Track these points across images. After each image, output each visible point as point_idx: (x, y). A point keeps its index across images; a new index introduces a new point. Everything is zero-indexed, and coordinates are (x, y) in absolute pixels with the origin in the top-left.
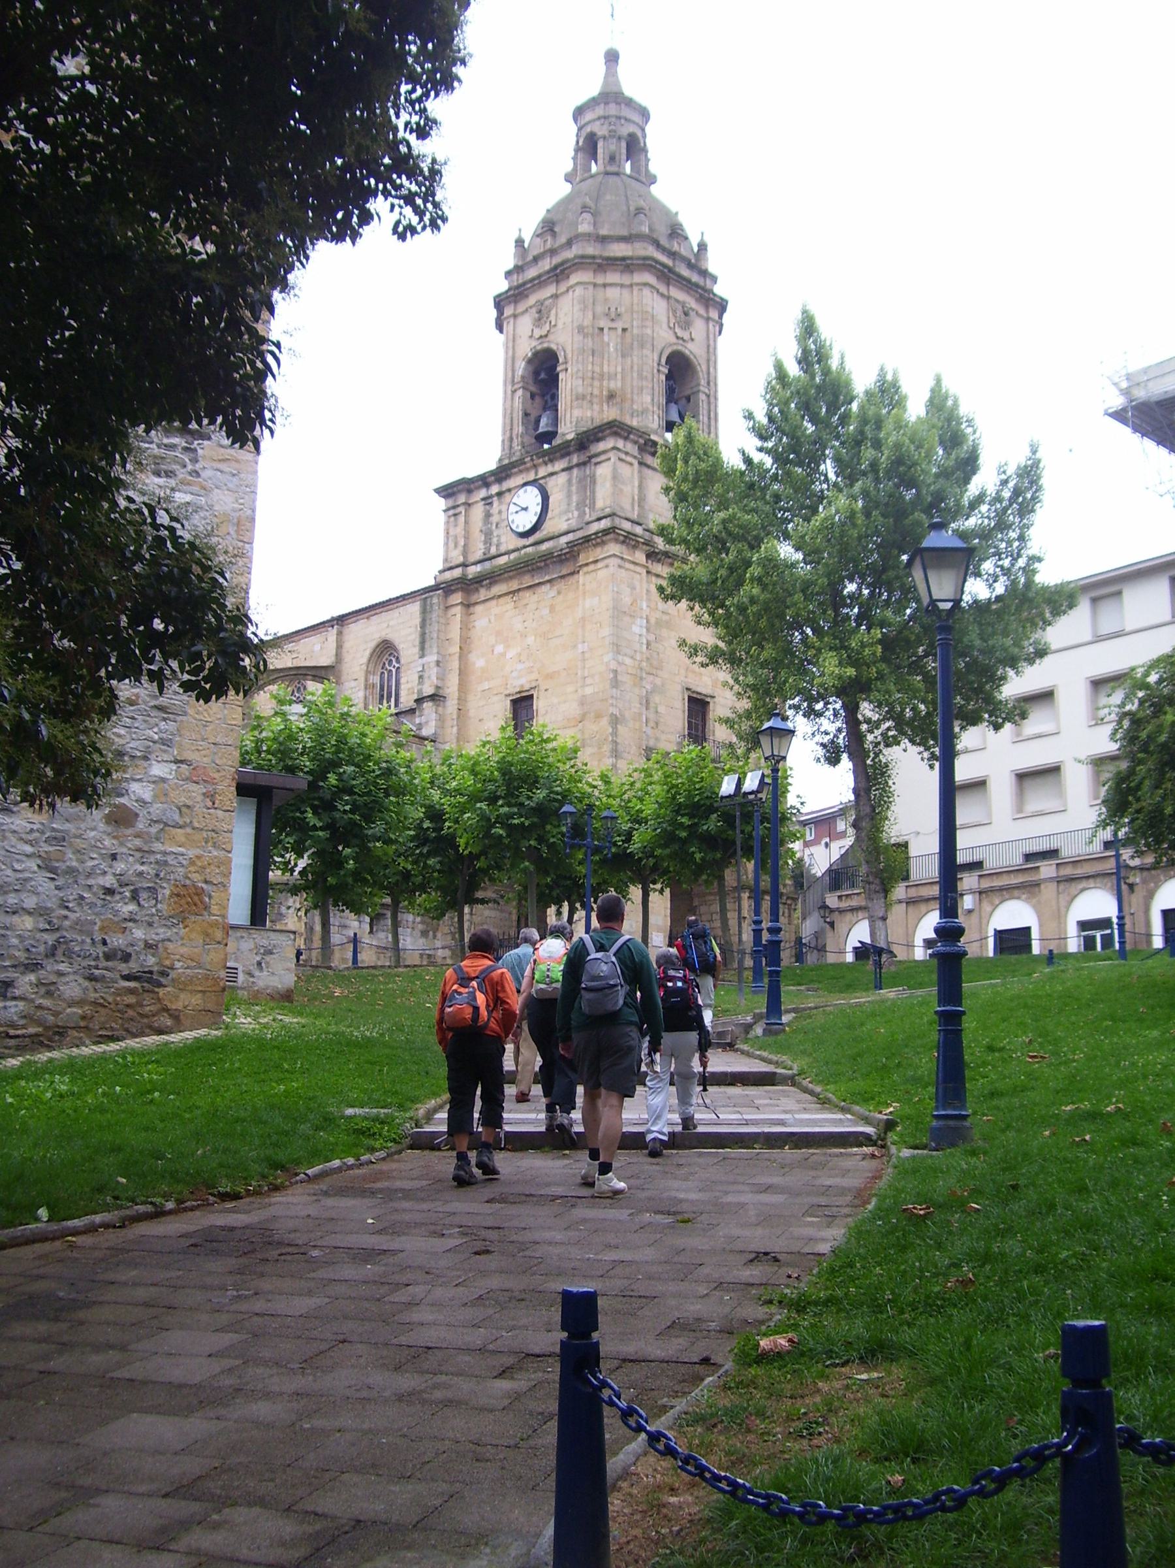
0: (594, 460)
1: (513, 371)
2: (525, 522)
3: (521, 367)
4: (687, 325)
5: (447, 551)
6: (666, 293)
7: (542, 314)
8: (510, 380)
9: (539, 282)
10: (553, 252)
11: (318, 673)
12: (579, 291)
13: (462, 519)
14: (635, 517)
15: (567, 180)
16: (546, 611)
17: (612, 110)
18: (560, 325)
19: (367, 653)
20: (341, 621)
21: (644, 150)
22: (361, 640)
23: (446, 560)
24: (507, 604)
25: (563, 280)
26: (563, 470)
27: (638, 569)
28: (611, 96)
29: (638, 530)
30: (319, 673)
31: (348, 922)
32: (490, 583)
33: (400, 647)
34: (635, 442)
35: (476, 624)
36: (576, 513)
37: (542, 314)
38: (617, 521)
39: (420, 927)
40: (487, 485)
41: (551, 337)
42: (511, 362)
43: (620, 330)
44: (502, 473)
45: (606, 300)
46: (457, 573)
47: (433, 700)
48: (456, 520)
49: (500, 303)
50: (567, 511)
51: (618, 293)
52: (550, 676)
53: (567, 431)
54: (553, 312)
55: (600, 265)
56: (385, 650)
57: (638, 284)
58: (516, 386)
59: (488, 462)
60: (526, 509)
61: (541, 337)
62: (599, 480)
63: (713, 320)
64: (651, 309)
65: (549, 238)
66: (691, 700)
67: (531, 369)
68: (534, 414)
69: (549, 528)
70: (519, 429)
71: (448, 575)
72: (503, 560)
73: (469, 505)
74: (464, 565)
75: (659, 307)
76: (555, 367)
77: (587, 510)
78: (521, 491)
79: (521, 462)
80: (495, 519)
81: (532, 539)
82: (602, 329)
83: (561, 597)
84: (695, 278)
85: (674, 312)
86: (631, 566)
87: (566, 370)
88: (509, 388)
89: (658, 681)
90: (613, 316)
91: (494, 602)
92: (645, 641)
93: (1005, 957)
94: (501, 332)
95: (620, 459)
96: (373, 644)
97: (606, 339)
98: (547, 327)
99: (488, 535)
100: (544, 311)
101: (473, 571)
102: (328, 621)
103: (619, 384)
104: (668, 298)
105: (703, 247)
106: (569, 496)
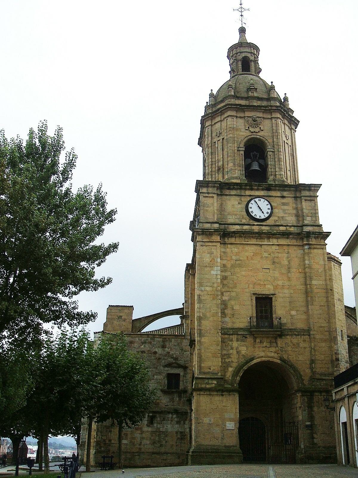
28: (243, 44)
39: (176, 419)
55: (212, 117)
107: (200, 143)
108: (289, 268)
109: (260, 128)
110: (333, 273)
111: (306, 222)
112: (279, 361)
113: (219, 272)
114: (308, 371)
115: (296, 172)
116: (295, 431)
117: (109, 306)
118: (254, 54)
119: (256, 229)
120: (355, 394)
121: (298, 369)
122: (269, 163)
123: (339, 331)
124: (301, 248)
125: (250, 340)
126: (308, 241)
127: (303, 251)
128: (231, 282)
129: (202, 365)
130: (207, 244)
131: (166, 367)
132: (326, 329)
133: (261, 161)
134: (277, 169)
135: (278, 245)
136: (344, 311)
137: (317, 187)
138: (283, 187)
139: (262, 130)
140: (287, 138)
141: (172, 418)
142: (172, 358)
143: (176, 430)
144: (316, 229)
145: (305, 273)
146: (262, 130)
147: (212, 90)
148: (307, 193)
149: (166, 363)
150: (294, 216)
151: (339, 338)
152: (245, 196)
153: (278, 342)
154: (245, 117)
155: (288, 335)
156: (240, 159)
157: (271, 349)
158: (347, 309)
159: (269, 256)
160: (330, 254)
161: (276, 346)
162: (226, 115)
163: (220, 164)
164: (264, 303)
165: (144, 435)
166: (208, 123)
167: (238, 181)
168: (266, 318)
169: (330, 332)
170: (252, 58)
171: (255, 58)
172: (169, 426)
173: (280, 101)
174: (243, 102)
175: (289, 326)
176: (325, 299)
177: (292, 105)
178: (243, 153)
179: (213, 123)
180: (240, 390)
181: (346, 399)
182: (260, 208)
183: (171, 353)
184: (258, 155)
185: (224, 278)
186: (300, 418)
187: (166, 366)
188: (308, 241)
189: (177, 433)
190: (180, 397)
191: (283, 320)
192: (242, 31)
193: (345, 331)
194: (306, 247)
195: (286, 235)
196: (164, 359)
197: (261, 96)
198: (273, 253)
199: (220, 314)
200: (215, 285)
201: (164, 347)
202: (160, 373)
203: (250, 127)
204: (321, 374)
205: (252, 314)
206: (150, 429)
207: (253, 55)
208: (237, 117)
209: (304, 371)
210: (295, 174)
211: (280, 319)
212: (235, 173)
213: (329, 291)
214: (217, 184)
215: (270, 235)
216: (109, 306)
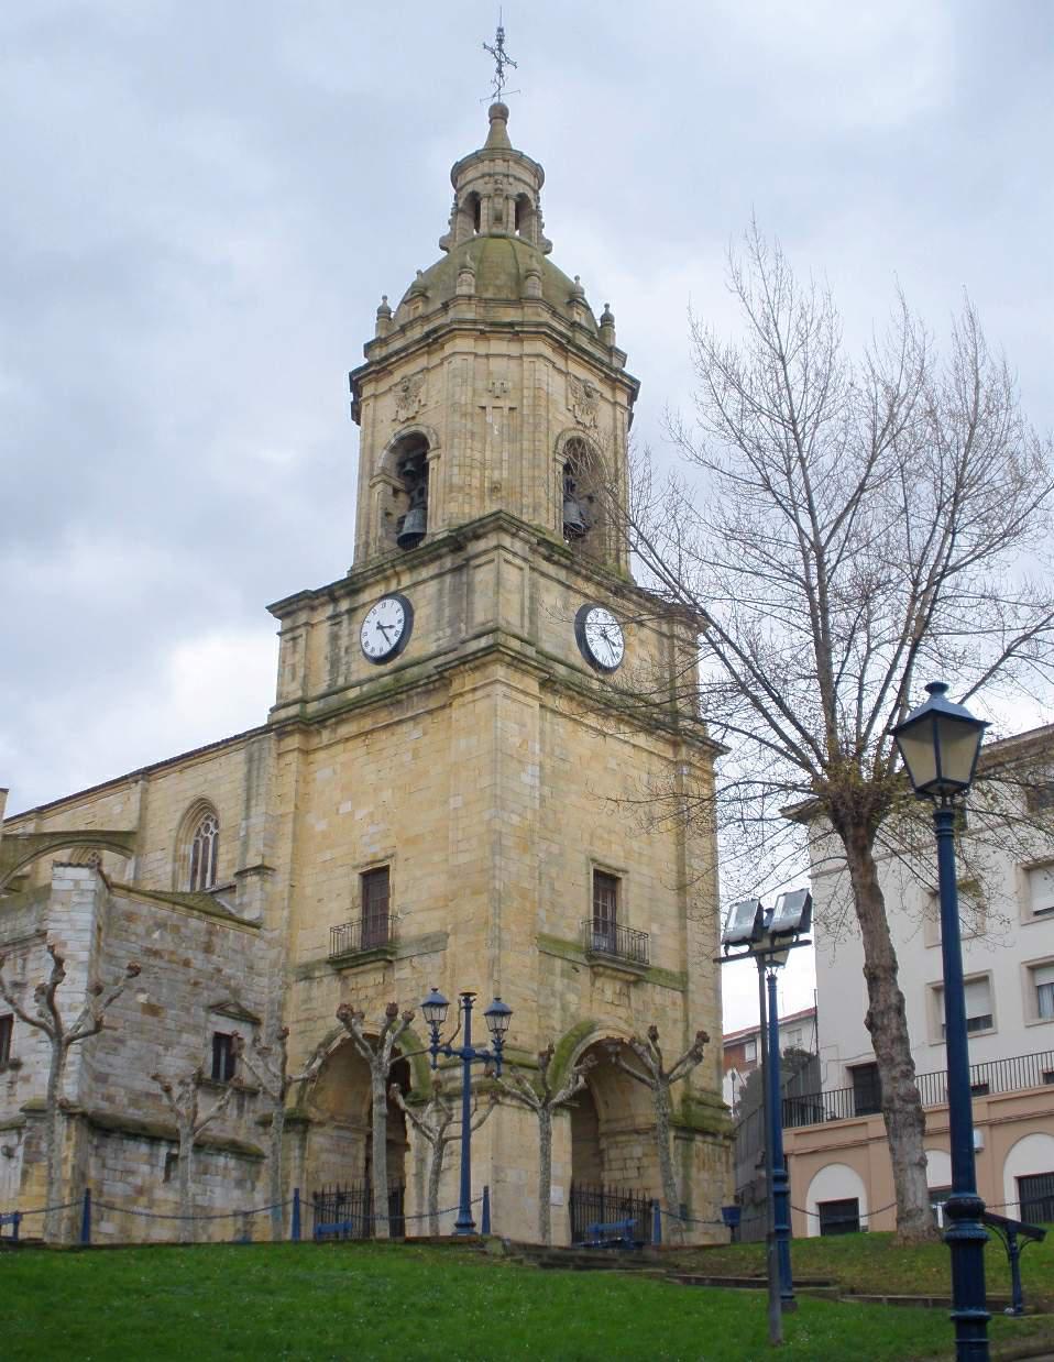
0: (474, 562)
1: (372, 463)
2: (378, 644)
3: (382, 458)
4: (591, 409)
5: (280, 684)
6: (563, 369)
7: (407, 391)
8: (368, 476)
9: (405, 354)
10: (425, 318)
11: (116, 840)
12: (457, 361)
13: (301, 642)
14: (525, 636)
15: (442, 248)
16: (407, 757)
17: (500, 166)
18: (432, 404)
19: (178, 815)
20: (148, 773)
21: (537, 214)
22: (171, 798)
23: (279, 696)
24: (357, 749)
25: (436, 350)
26: (432, 578)
27: (529, 700)
28: (497, 148)
29: (530, 651)
30: (121, 841)
31: (133, 1166)
32: (337, 723)
33: (220, 806)
34: (527, 542)
35: (317, 775)
36: (448, 631)
37: (407, 391)
38: (502, 638)
40: (334, 600)
41: (420, 419)
42: (368, 452)
43: (506, 410)
44: (351, 586)
45: (490, 374)
46: (293, 710)
47: (259, 873)
48: (294, 646)
49: (357, 381)
50: (438, 628)
51: (502, 362)
52: (412, 841)
53: (437, 529)
54: (423, 389)
56: (203, 810)
57: (529, 355)
58: (375, 480)
59: (338, 567)
60: (380, 627)
61: (408, 419)
62: (479, 588)
63: (622, 406)
64: (552, 382)
65: (420, 304)
66: (597, 874)
67: (395, 458)
68: (397, 514)
69: (414, 650)
70: (377, 531)
71: (283, 714)
72: (352, 694)
73: (312, 625)
74: (303, 701)
75: (556, 385)
76: (425, 454)
77: (463, 626)
78: (378, 607)
79: (380, 569)
80: (344, 642)
81: (390, 666)
82: (484, 408)
83: (426, 740)
84: (598, 353)
85: (575, 391)
86: (521, 697)
87: (439, 457)
88: (366, 482)
89: (555, 849)
90: (498, 392)
91: (340, 747)
92: (537, 795)
93: (831, 1239)
94: (358, 423)
95: (507, 561)
96: (187, 804)
97: (489, 419)
98: (416, 406)
99: (334, 663)
100: (412, 389)
101: (312, 708)
102: (132, 775)
103: (505, 474)
104: (567, 374)
105: (607, 319)
106: (440, 610)
125: (584, 976)
141: (226, 1168)
149: (212, 1002)
172: (218, 1191)
183: (227, 971)
196: (207, 988)
201: (208, 949)
202: (197, 1029)
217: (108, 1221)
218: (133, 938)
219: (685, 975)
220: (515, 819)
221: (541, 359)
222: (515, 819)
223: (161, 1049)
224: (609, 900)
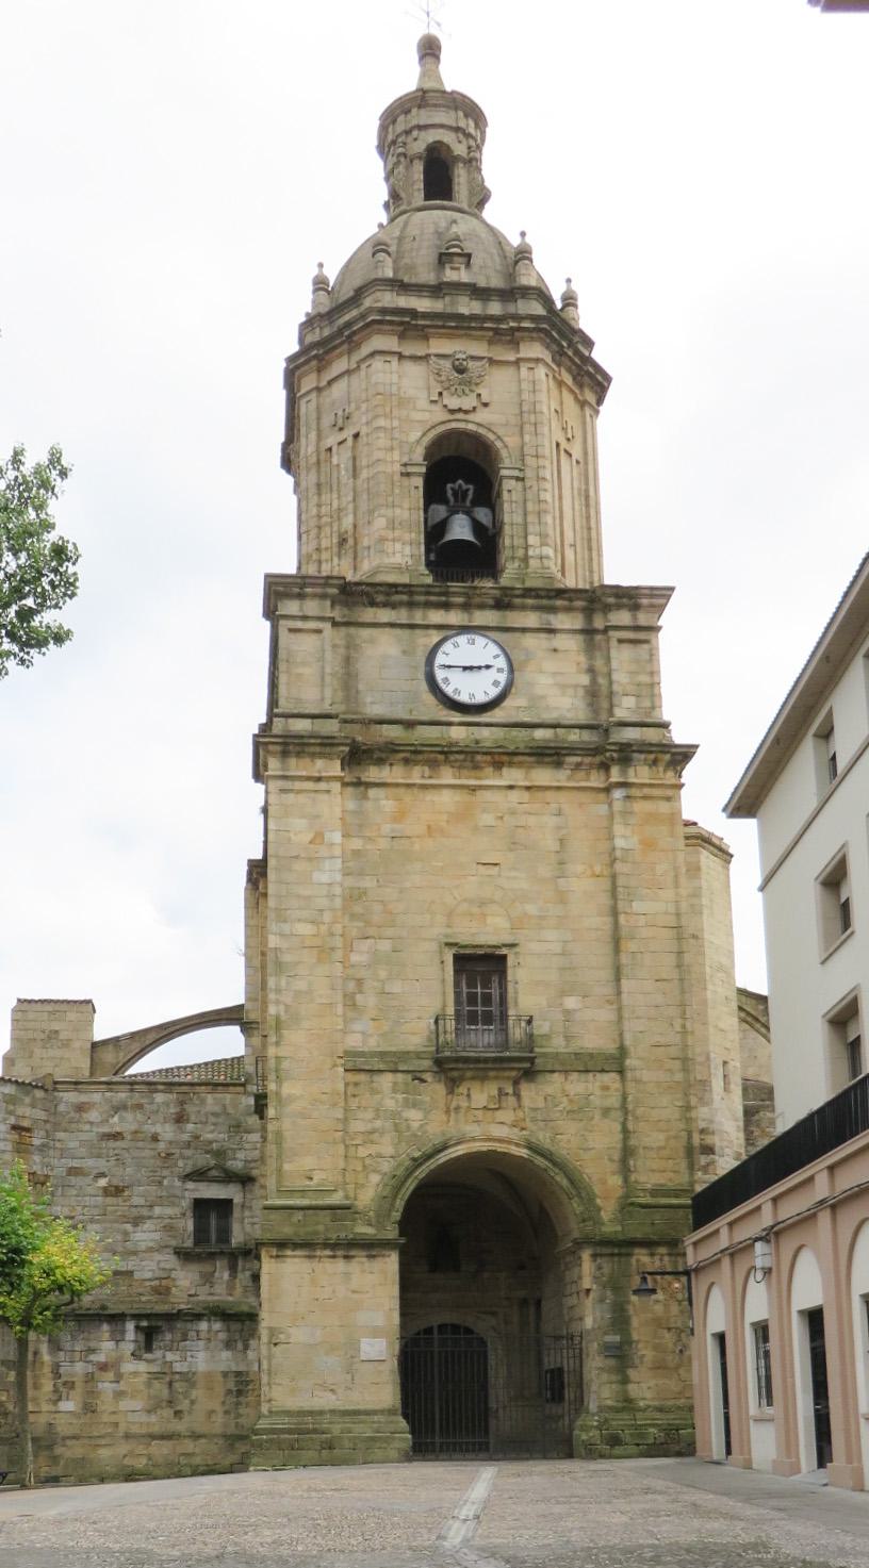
34: (323, 596)
107: (288, 463)
108: (561, 863)
109: (479, 395)
110: (704, 885)
111: (621, 713)
112: (523, 1152)
113: (338, 877)
114: (616, 1181)
115: (594, 554)
116: (571, 1361)
117: (19, 1000)
118: (468, 136)
119: (458, 734)
120: (752, 1245)
121: (585, 1176)
122: (507, 519)
123: (716, 1060)
124: (602, 796)
126: (624, 772)
127: (606, 806)
128: (377, 908)
129: (287, 1167)
130: (298, 785)
131: (190, 1180)
132: (674, 1052)
133: (483, 515)
134: (532, 540)
135: (528, 788)
136: (734, 1006)
137: (659, 596)
138: (551, 597)
139: (486, 405)
140: (566, 433)
142: (207, 1152)
143: (223, 1367)
144: (651, 735)
145: (614, 877)
146: (486, 405)
147: (321, 265)
148: (622, 617)
150: (581, 692)
151: (717, 1084)
152: (427, 627)
153: (522, 1093)
154: (427, 356)
155: (553, 1072)
156: (408, 504)
157: (500, 1115)
158: (744, 999)
159: (499, 822)
160: (695, 824)
161: (516, 1105)
162: (365, 350)
163: (348, 522)
164: (480, 971)
165: (122, 1386)
166: (308, 382)
167: (405, 579)
168: (488, 1019)
169: (686, 1062)
170: (459, 149)
171: (469, 148)
172: (201, 1356)
173: (547, 300)
174: (423, 304)
175: (558, 1044)
176: (671, 960)
177: (587, 319)
178: (420, 482)
179: (323, 383)
180: (403, 1241)
181: (726, 1262)
182: (472, 664)
184: (471, 493)
185: (354, 896)
186: (589, 1323)
187: (188, 1177)
188: (624, 772)
189: (225, 1374)
190: (233, 1269)
191: (540, 1026)
192: (430, 49)
193: (735, 1063)
194: (618, 794)
195: (550, 755)
197: (482, 283)
198: (513, 813)
199: (340, 1010)
200: (327, 917)
201: (180, 1119)
202: (171, 1199)
203: (445, 393)
204: (655, 1192)
205: (444, 1006)
206: (142, 1367)
207: (464, 141)
208: (401, 356)
209: (604, 1182)
210: (591, 559)
211: (529, 1022)
212: (398, 552)
213: (688, 945)
214: (332, 586)
215: (501, 758)
216: (19, 1000)
217: (68, 1399)
218: (87, 1127)
219: (623, 1051)
220: (305, 929)
221: (378, 357)
222: (305, 929)
223: (129, 1227)
224: (495, 984)
